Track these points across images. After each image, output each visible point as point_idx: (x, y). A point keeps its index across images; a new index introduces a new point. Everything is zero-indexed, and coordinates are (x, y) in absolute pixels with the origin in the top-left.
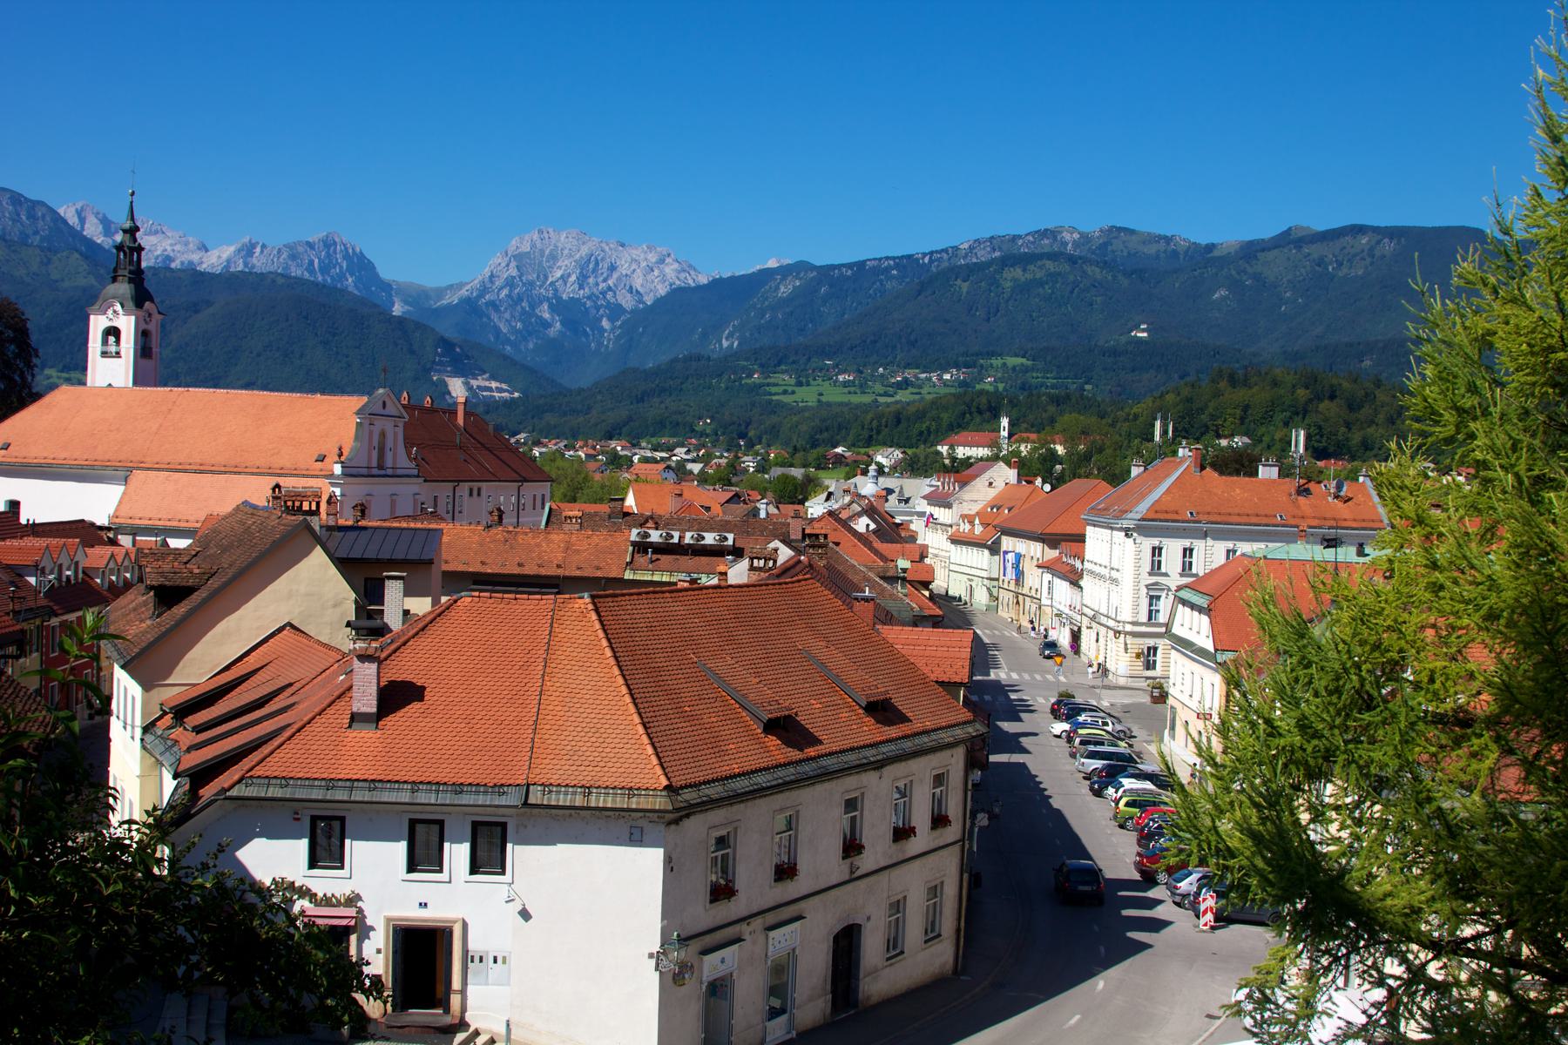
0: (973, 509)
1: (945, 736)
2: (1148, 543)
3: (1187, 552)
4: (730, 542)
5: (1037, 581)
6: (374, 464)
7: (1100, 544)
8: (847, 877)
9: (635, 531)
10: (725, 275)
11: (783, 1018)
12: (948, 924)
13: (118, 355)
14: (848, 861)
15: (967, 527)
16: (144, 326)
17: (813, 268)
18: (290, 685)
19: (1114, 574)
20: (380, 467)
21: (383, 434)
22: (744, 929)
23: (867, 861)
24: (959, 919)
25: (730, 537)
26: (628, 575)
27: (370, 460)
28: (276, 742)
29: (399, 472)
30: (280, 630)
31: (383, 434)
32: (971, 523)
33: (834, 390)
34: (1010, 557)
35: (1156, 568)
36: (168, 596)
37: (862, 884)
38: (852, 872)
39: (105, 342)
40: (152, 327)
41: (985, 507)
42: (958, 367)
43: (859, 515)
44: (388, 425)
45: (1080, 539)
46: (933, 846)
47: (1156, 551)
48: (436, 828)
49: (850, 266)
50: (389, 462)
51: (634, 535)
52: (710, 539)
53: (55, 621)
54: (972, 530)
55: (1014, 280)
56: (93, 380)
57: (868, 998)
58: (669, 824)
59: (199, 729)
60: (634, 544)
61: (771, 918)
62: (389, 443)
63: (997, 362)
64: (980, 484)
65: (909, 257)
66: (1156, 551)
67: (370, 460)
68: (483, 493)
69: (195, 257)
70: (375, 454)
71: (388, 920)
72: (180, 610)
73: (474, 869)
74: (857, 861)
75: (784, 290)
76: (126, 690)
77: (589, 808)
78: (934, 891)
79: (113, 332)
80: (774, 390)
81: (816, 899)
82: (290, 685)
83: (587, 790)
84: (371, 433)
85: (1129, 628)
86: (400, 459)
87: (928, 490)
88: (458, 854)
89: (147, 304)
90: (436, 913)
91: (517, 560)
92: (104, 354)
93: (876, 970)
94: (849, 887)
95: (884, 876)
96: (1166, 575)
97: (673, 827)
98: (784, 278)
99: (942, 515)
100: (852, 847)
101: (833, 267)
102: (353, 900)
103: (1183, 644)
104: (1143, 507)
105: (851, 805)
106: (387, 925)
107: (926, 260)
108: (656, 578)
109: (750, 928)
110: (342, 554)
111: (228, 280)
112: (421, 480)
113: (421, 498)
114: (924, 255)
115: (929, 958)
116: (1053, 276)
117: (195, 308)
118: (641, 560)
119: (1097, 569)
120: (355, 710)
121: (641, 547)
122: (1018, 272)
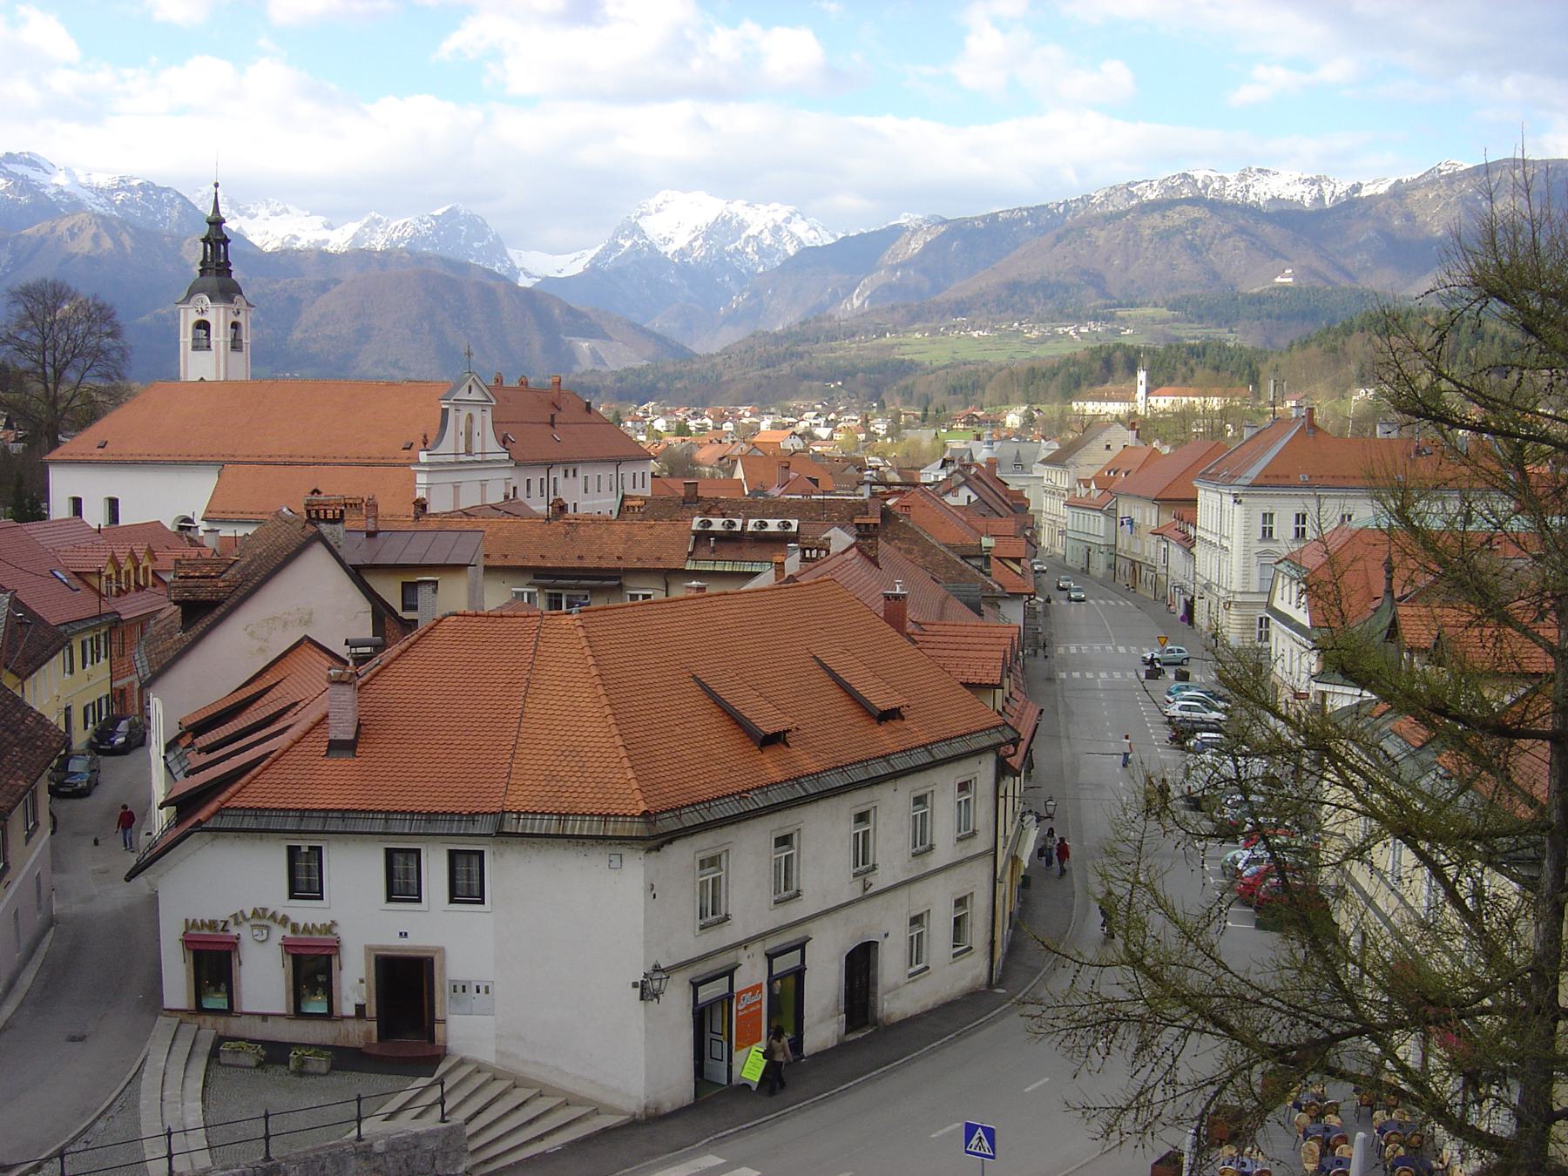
0: (1090, 473)
1: (975, 744)
2: (1262, 504)
5: (1153, 548)
9: (697, 520)
12: (977, 934)
15: (1084, 492)
19: (1225, 543)
21: (470, 416)
23: (880, 880)
25: (795, 523)
26: (690, 566)
28: (258, 769)
29: (489, 457)
31: (470, 416)
32: (1087, 487)
33: (974, 342)
35: (1267, 534)
38: (865, 889)
40: (241, 319)
41: (1103, 471)
42: (1096, 320)
44: (477, 413)
45: (1193, 502)
47: (1268, 517)
49: (983, 219)
50: (477, 448)
51: (696, 524)
52: (773, 525)
56: (186, 373)
57: (888, 1017)
58: (649, 851)
59: (209, 749)
60: (697, 534)
62: (477, 428)
65: (1045, 207)
66: (1268, 517)
68: (579, 473)
70: (462, 440)
71: (369, 949)
73: (454, 898)
77: (564, 836)
79: (203, 325)
80: (907, 348)
81: (825, 920)
83: (562, 816)
85: (1239, 598)
88: (280, 917)
92: (195, 348)
93: (897, 987)
94: (863, 906)
102: (328, 929)
103: (1285, 619)
104: (1253, 472)
107: (1061, 209)
109: (749, 951)
116: (1195, 222)
117: (323, 288)
119: (1209, 537)
120: (332, 737)
121: (702, 537)
122: (1156, 219)
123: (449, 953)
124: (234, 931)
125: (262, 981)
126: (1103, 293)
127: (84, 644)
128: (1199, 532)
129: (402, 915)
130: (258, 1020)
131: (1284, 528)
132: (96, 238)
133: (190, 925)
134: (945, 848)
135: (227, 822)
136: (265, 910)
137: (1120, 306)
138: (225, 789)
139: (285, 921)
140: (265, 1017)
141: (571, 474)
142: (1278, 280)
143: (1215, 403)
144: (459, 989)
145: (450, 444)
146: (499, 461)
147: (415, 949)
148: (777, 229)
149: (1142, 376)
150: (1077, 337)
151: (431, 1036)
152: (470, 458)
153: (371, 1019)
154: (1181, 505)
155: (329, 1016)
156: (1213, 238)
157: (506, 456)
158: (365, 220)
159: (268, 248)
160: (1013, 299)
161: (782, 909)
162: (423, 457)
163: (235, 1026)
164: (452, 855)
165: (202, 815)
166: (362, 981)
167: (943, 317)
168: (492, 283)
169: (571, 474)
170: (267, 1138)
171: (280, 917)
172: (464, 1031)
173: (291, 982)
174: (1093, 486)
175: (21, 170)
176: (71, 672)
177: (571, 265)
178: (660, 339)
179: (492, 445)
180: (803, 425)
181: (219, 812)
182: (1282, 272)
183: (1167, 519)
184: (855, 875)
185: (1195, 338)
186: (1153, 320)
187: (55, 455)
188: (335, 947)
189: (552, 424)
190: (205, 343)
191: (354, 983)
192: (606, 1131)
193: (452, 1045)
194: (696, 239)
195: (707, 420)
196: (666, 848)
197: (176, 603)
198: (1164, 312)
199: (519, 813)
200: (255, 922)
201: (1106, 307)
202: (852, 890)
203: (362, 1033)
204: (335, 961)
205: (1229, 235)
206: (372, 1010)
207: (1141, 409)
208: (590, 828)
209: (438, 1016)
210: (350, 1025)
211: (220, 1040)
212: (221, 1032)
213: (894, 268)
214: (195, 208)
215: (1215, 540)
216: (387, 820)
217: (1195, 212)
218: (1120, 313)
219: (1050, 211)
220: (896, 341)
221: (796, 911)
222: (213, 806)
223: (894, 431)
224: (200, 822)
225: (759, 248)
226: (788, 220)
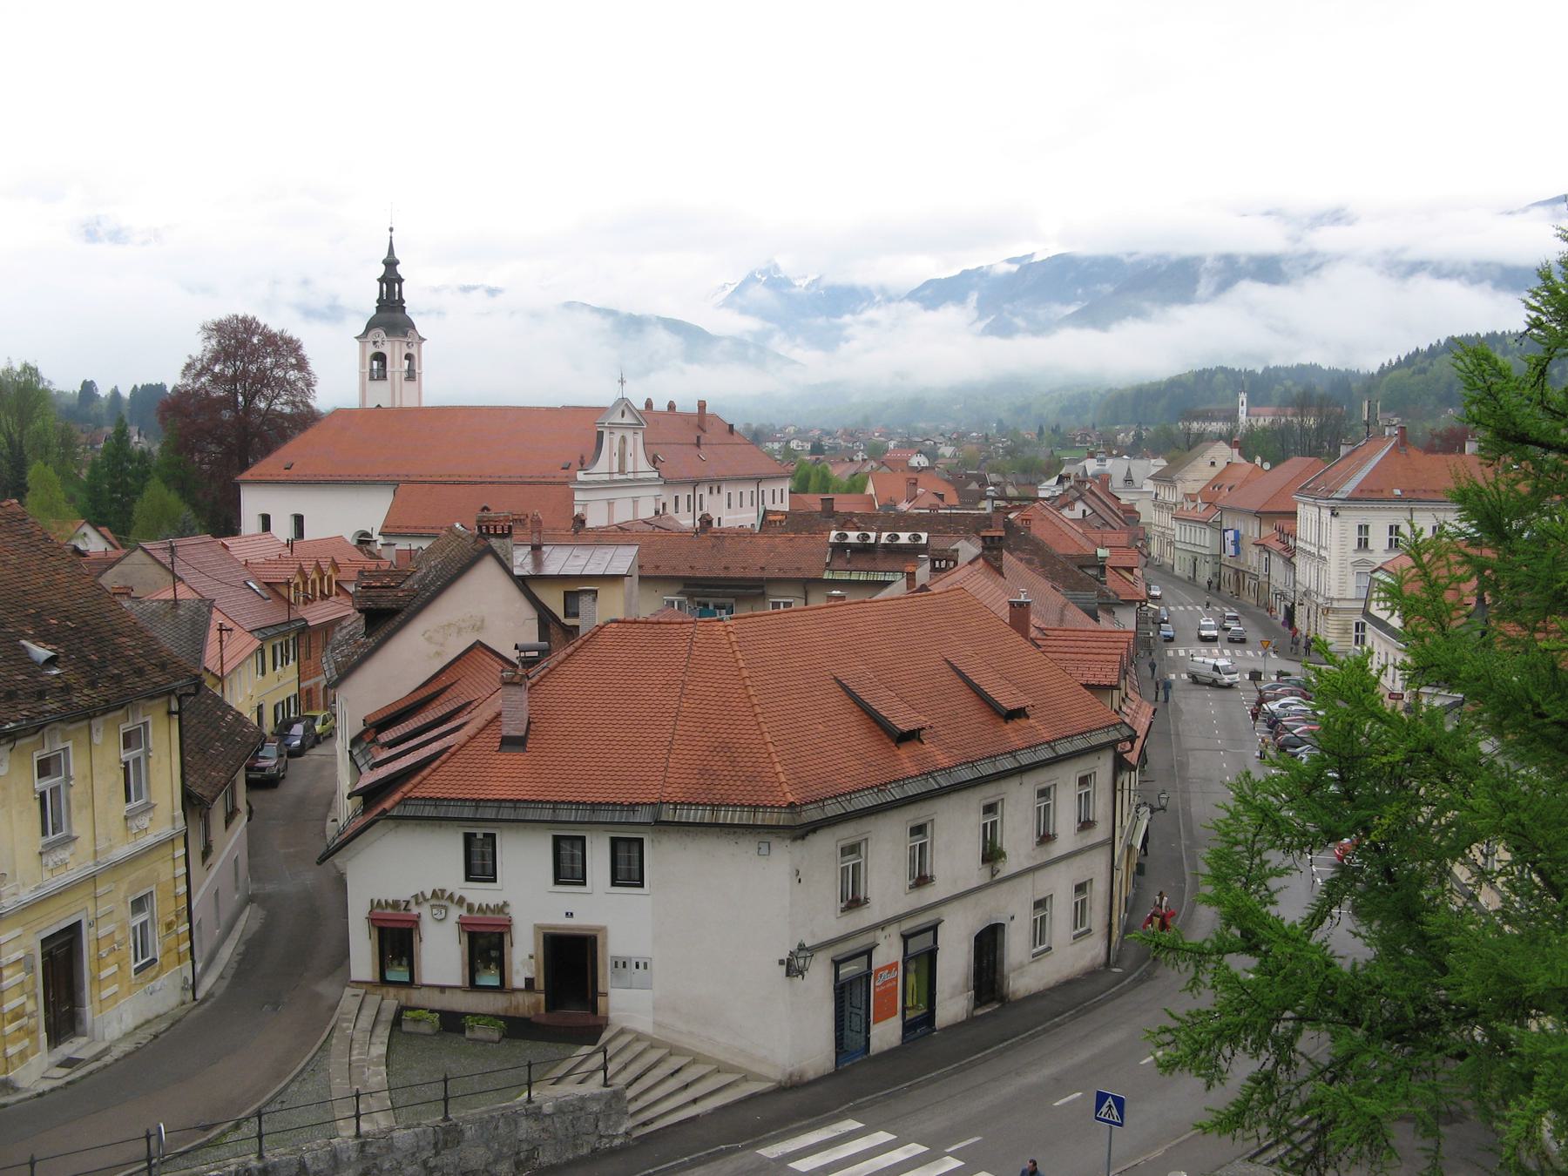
0: (1194, 488)
4: (924, 541)
5: (1255, 558)
7: (1309, 519)
8: (988, 880)
9: (834, 533)
13: (385, 377)
19: (1323, 553)
21: (623, 439)
23: (1008, 867)
25: (924, 536)
26: (827, 575)
29: (640, 476)
31: (623, 439)
34: (1230, 535)
35: (1363, 544)
37: (1005, 887)
38: (993, 875)
44: (629, 435)
45: (1293, 515)
46: (1079, 846)
47: (1364, 529)
48: (579, 844)
50: (629, 467)
52: (904, 538)
59: (392, 744)
60: (834, 546)
62: (629, 449)
66: (1364, 529)
70: (616, 460)
71: (538, 927)
81: (956, 905)
87: (1154, 471)
90: (584, 919)
93: (1021, 966)
94: (990, 891)
99: (1167, 495)
103: (1381, 624)
106: (536, 933)
108: (854, 577)
113: (663, 499)
115: (1072, 954)
118: (838, 563)
119: (1308, 548)
124: (415, 910)
125: (441, 956)
127: (274, 648)
129: (569, 897)
130: (437, 992)
133: (376, 905)
136: (443, 891)
139: (461, 900)
140: (442, 988)
144: (620, 965)
145: (604, 465)
146: (650, 480)
151: (595, 1009)
153: (539, 992)
155: (502, 988)
161: (916, 894)
162: (581, 476)
163: (416, 997)
164: (614, 842)
172: (625, 1004)
176: (263, 673)
181: (404, 801)
187: (246, 475)
188: (508, 926)
191: (524, 959)
199: (675, 804)
203: (529, 1004)
204: (507, 939)
206: (540, 984)
209: (600, 989)
211: (401, 1010)
215: (1314, 550)
221: (929, 895)
222: (397, 797)
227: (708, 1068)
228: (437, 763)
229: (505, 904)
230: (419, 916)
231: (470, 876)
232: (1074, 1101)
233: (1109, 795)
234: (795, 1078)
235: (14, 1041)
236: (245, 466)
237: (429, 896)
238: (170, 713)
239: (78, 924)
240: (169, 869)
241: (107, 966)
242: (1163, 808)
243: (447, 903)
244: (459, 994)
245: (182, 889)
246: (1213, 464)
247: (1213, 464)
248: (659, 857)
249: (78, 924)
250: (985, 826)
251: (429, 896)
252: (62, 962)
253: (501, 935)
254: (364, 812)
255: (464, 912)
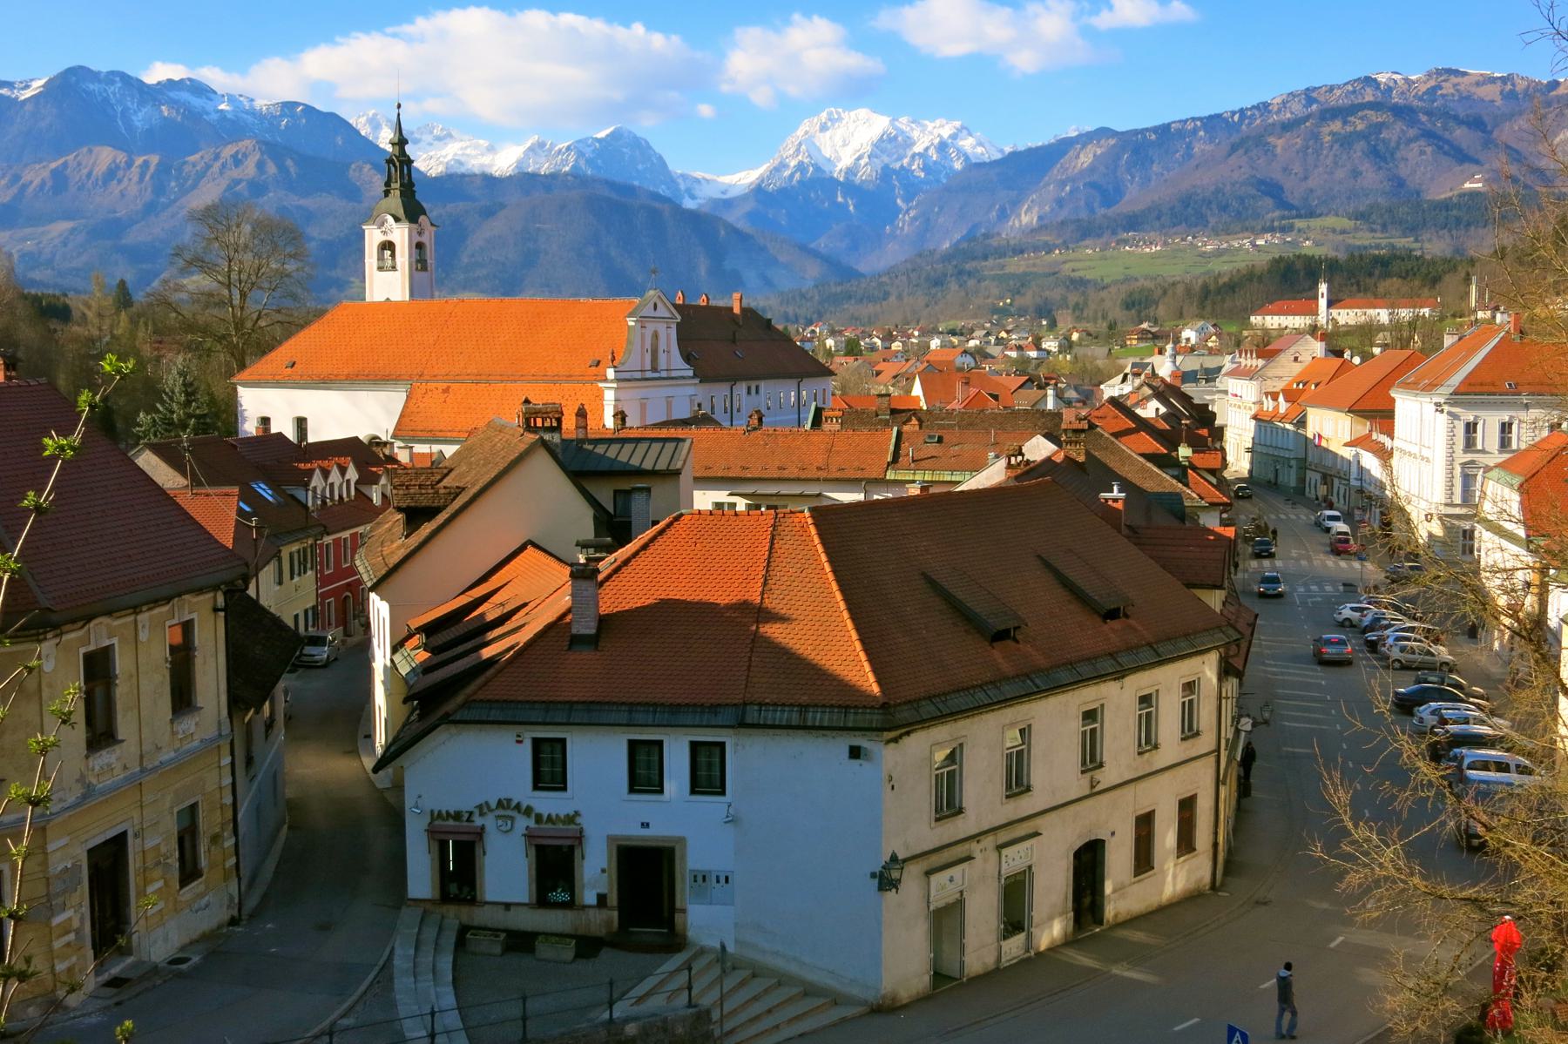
3: (1506, 428)
6: (648, 367)
8: (1087, 792)
10: (1021, 147)
11: (1021, 937)
13: (394, 268)
14: (1088, 775)
16: (417, 239)
17: (1114, 134)
18: (525, 605)
19: (1426, 453)
20: (654, 369)
21: (656, 335)
22: (975, 847)
23: (1108, 776)
24: (1216, 834)
26: (890, 475)
27: (643, 363)
29: (674, 374)
30: (522, 548)
31: (656, 335)
33: (1147, 256)
36: (415, 516)
38: (1093, 787)
39: (381, 258)
40: (425, 239)
41: (1291, 384)
42: (1272, 230)
43: (1147, 399)
44: (661, 328)
47: (1471, 428)
49: (1155, 130)
50: (662, 364)
53: (328, 539)
54: (1276, 408)
55: (1332, 133)
61: (1004, 836)
62: (662, 346)
63: (1316, 223)
64: (1285, 359)
65: (1218, 116)
66: (1471, 428)
67: (643, 363)
68: (762, 390)
69: (486, 160)
70: (648, 357)
71: (611, 839)
72: (427, 529)
74: (1098, 775)
75: (1085, 159)
76: (379, 609)
78: (1187, 806)
79: (388, 246)
81: (1053, 815)
82: (525, 605)
83: (804, 708)
84: (643, 336)
86: (673, 359)
88: (524, 807)
89: (422, 218)
91: (777, 463)
92: (380, 269)
95: (1129, 789)
96: (1483, 451)
97: (892, 745)
98: (1084, 146)
100: (1091, 759)
101: (1136, 132)
102: (570, 819)
104: (1457, 379)
105: (1090, 716)
107: (1236, 118)
109: (981, 846)
110: (575, 467)
111: (525, 181)
112: (697, 381)
114: (1234, 113)
116: (1380, 126)
117: (489, 213)
122: (1336, 126)
123: (690, 843)
124: (478, 821)
125: (506, 874)
126: (1283, 204)
127: (291, 555)
128: (1397, 443)
129: (644, 805)
130: (501, 910)
131: (1488, 436)
132: (260, 165)
133: (436, 816)
134: (1170, 744)
135: (466, 715)
136: (509, 801)
137: (1299, 216)
138: (468, 683)
139: (528, 811)
140: (507, 906)
141: (753, 390)
142: (1467, 185)
143: (1405, 314)
144: (700, 879)
147: (656, 839)
148: (942, 146)
149: (1323, 288)
150: (1256, 248)
151: (671, 924)
152: (656, 375)
153: (611, 908)
154: (1380, 415)
155: (570, 905)
156: (1398, 144)
157: (691, 373)
158: (528, 144)
159: (433, 173)
160: (1188, 213)
161: (1012, 804)
163: (481, 916)
164: (695, 746)
165: (449, 707)
166: (603, 871)
167: (1114, 233)
168: (657, 205)
169: (753, 390)
170: (524, 1019)
171: (524, 807)
172: (703, 920)
173: (534, 872)
174: (1281, 398)
175: (185, 96)
176: (280, 583)
177: (742, 178)
178: (827, 260)
179: (678, 361)
180: (972, 343)
181: (466, 704)
182: (1471, 178)
183: (1363, 428)
184: (1083, 772)
185: (1378, 247)
186: (1334, 231)
188: (580, 837)
189: (734, 341)
190: (389, 263)
191: (595, 872)
192: (844, 1020)
193: (690, 934)
194: (860, 158)
195: (876, 340)
196: (906, 740)
197: (399, 509)
198: (1347, 223)
199: (760, 704)
200: (501, 812)
201: (1283, 218)
202: (1079, 786)
203: (603, 921)
204: (577, 853)
205: (1416, 139)
206: (613, 900)
207: (1322, 319)
208: (830, 720)
209: (678, 905)
210: (591, 912)
211: (464, 930)
212: (465, 920)
213: (1063, 183)
214: (358, 132)
215: (1414, 449)
216: (630, 712)
217: (1375, 117)
218: (1299, 224)
219: (1226, 120)
220: (1064, 258)
221: (1026, 805)
222: (460, 698)
223: (1067, 346)
224: (447, 715)
225: (925, 165)
226: (954, 137)
227: (795, 991)
228: (481, 680)
229: (577, 814)
230: (483, 828)
231: (539, 783)
232: (1191, 1027)
233: (1214, 703)
234: (888, 1002)
235: (63, 958)
236: (242, 366)
237: (493, 805)
238: (216, 610)
239: (124, 834)
240: (214, 780)
241: (152, 881)
242: (1266, 722)
243: (514, 813)
244: (525, 909)
245: (228, 800)
246: (1296, 359)
247: (1296, 359)
248: (747, 756)
249: (124, 834)
250: (1084, 733)
251: (493, 805)
252: (108, 869)
253: (572, 848)
254: (421, 717)
255: (532, 823)
